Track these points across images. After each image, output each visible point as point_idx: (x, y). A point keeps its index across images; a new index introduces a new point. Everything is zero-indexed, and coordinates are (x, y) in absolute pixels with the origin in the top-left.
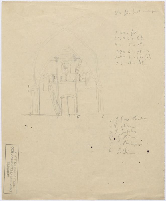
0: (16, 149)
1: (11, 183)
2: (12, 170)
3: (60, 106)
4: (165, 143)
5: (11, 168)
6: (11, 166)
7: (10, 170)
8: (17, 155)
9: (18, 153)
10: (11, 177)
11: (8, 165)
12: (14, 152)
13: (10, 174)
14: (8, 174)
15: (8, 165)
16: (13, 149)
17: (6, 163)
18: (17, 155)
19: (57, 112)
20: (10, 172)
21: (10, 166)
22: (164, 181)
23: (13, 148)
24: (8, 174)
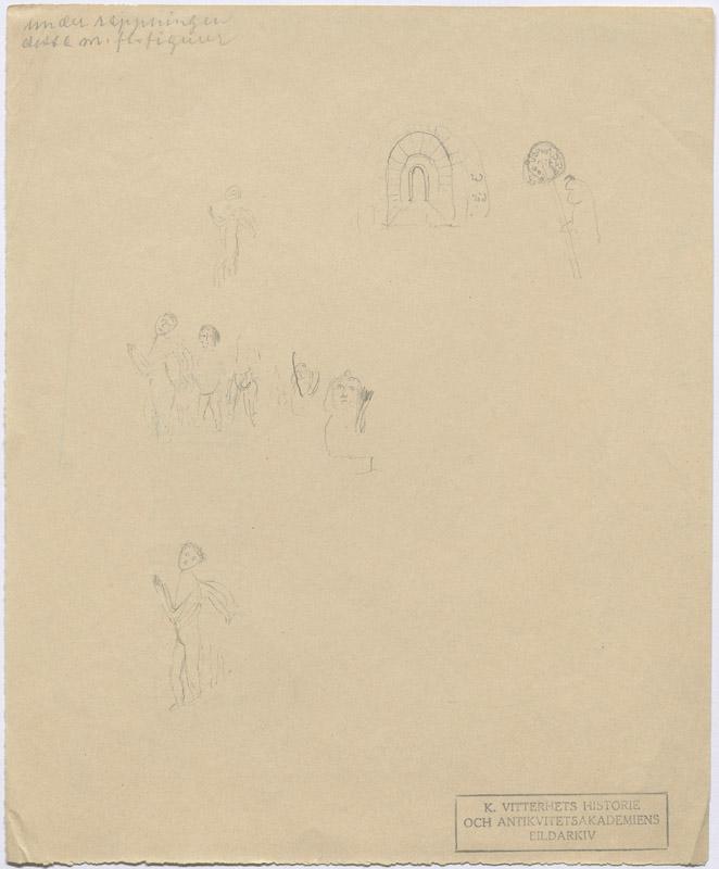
0: (472, 808)
1: (622, 820)
2: (563, 806)
3: (330, 393)
4: (3, 744)
5: (555, 823)
6: (549, 823)
7: (564, 829)
8: (496, 803)
9: (488, 800)
10: (596, 821)
11: (546, 836)
12: (487, 815)
13: (583, 827)
14: (582, 835)
15: (546, 836)
16: (473, 822)
17: (539, 845)
18: (496, 803)
19: (333, 395)
20: (574, 828)
21: (550, 828)
22: (5, 473)
23: (468, 823)
24: (582, 835)
